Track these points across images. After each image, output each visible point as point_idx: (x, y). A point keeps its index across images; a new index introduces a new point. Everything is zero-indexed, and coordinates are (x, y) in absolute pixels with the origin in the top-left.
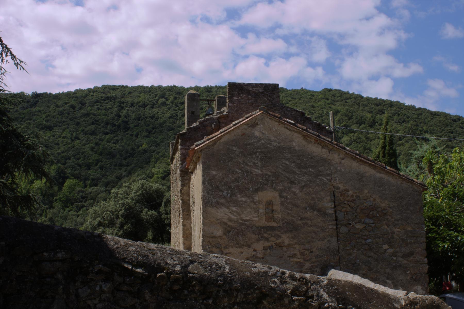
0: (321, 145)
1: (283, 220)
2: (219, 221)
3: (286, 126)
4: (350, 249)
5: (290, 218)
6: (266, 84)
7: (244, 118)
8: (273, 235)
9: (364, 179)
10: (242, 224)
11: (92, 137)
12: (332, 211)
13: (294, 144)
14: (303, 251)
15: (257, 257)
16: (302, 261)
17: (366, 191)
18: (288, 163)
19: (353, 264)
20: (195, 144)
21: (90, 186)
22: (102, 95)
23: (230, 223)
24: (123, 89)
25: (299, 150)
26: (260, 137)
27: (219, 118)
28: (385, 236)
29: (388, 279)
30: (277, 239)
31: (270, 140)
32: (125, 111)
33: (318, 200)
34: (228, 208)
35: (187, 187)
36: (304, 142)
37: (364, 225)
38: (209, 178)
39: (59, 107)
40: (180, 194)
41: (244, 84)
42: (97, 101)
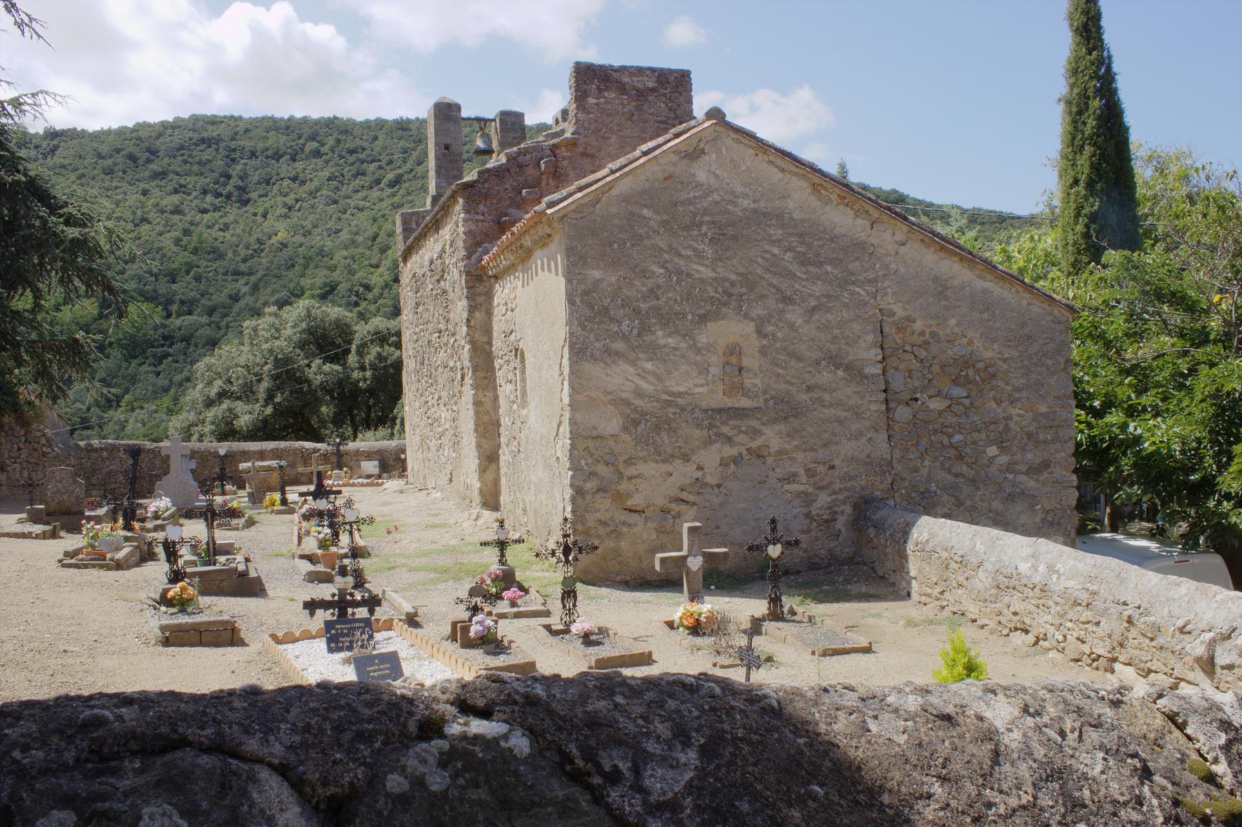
1: (765, 392)
2: (610, 397)
3: (772, 158)
6: (662, 69)
7: (668, 136)
8: (743, 429)
9: (949, 293)
10: (669, 404)
11: (177, 218)
12: (877, 370)
13: (791, 204)
15: (706, 485)
16: (811, 490)
17: (953, 322)
18: (776, 251)
19: (922, 493)
20: (546, 199)
21: (179, 316)
22: (191, 134)
24: (232, 123)
25: (802, 221)
28: (992, 427)
30: (753, 439)
31: (732, 192)
32: (239, 167)
33: (847, 344)
34: (633, 363)
35: (483, 313)
36: (814, 202)
37: (948, 403)
38: (583, 287)
39: (103, 158)
40: (465, 329)
42: (182, 148)
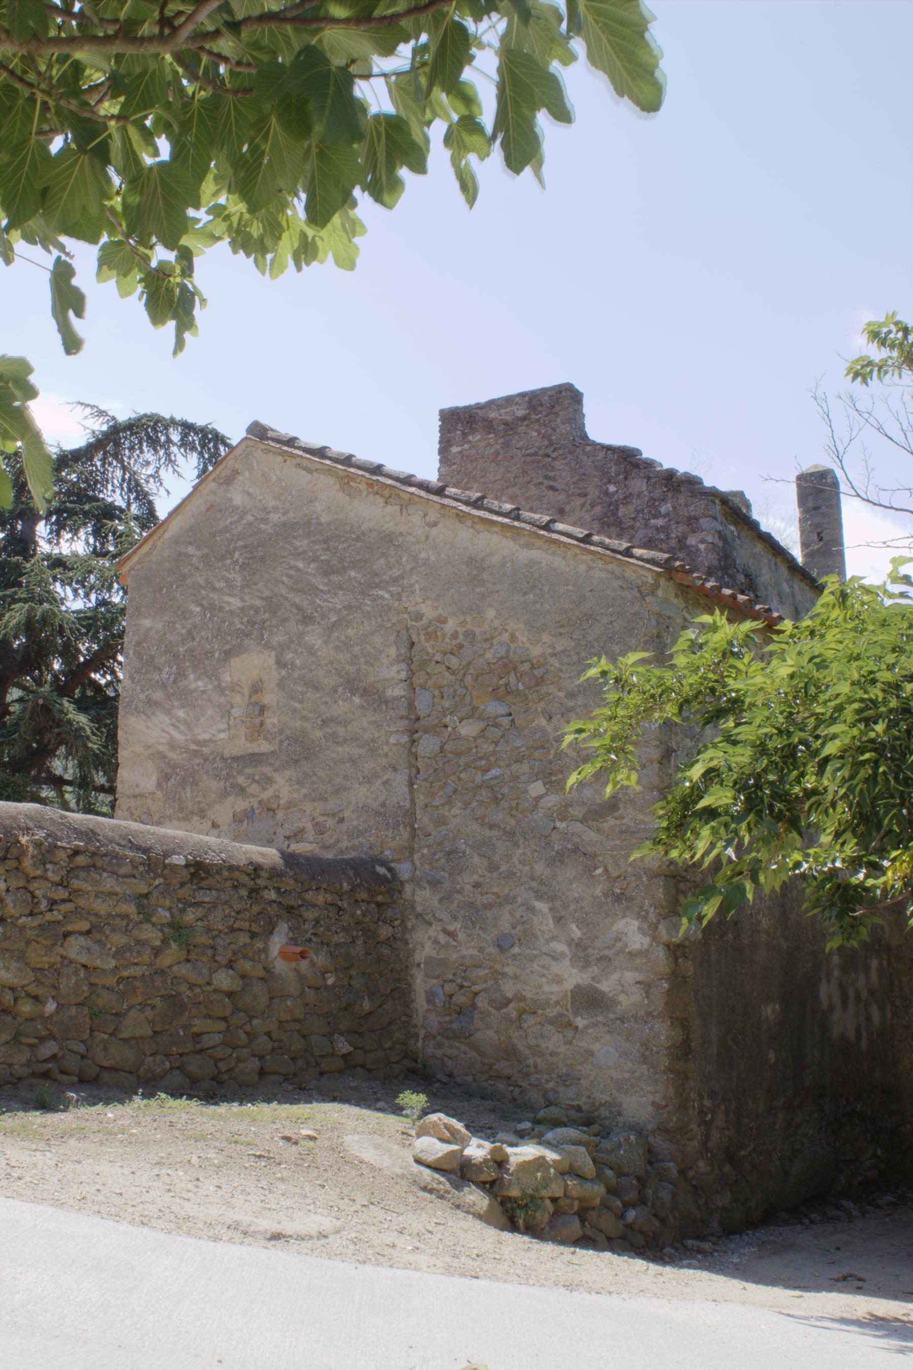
0: (382, 496)
1: (281, 732)
4: (442, 805)
5: (298, 724)
8: (257, 777)
9: (485, 576)
10: (195, 754)
12: (397, 691)
13: (319, 507)
14: (321, 819)
18: (300, 565)
19: (449, 854)
23: (171, 755)
25: (329, 524)
28: (537, 754)
29: (539, 896)
30: (264, 789)
33: (367, 662)
34: (168, 712)
36: (342, 498)
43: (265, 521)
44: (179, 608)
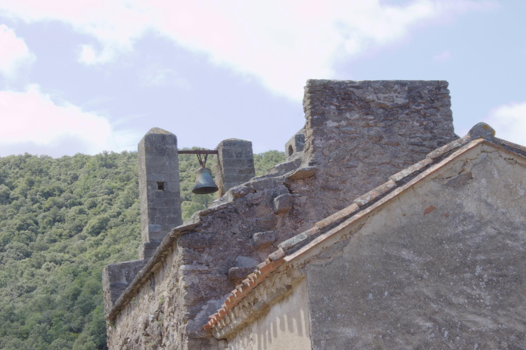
26: (482, 218)
27: (291, 179)
41: (352, 84)
43: (514, 237)
44: (398, 320)
